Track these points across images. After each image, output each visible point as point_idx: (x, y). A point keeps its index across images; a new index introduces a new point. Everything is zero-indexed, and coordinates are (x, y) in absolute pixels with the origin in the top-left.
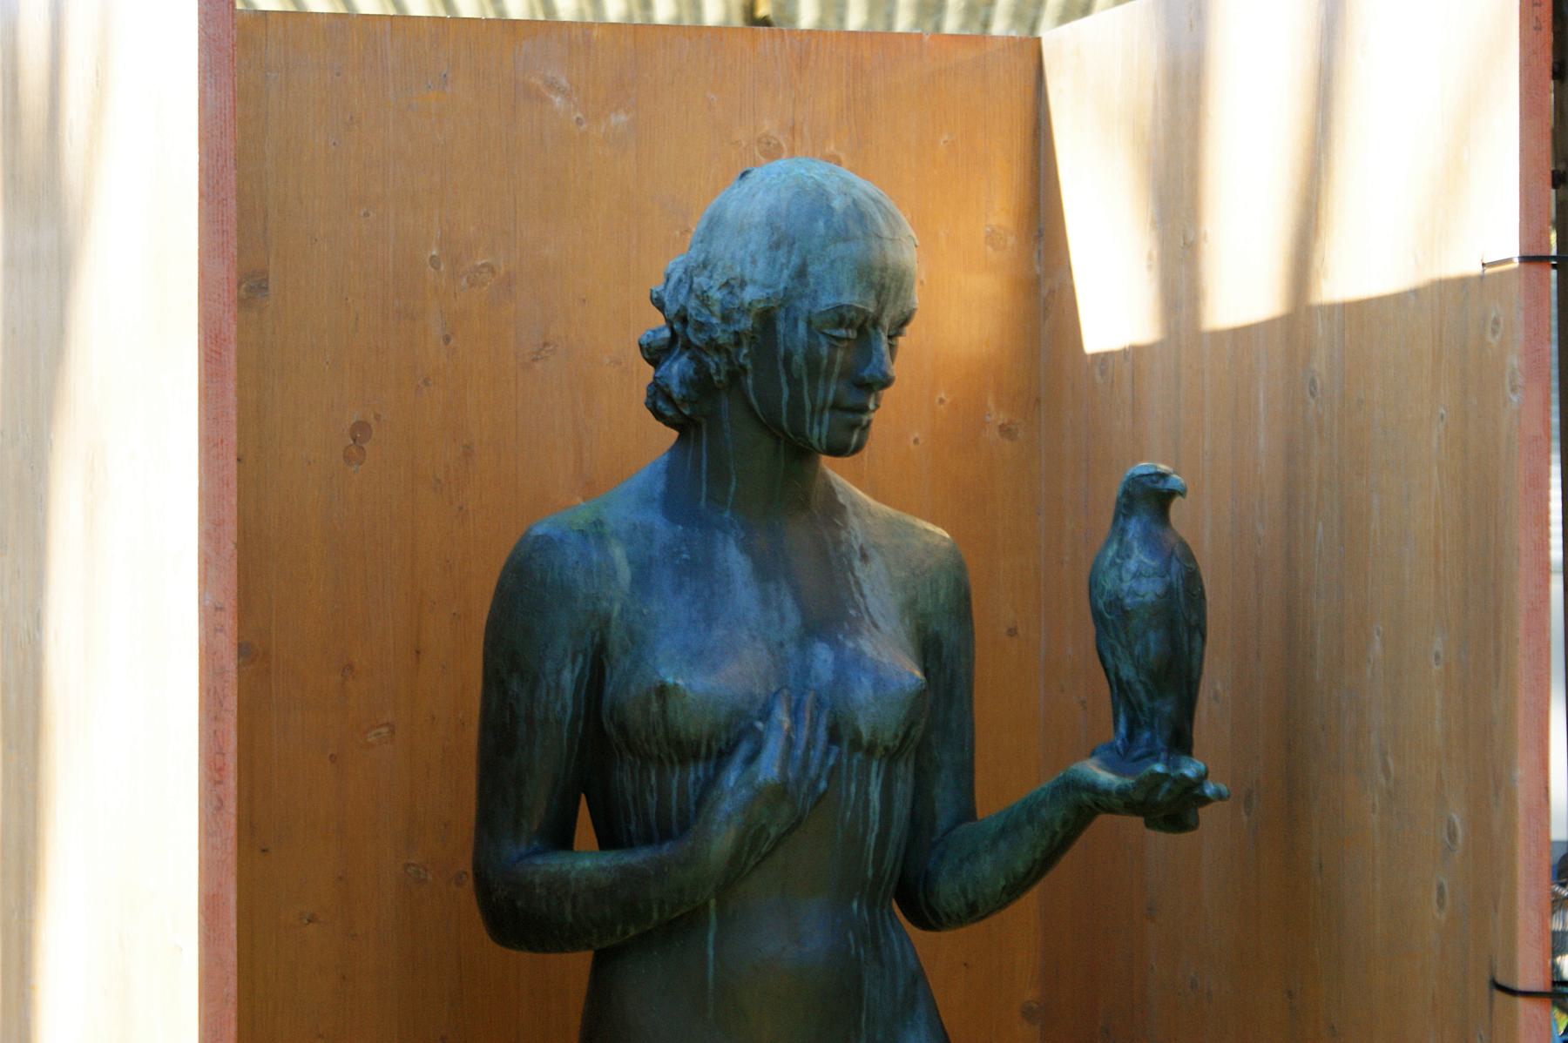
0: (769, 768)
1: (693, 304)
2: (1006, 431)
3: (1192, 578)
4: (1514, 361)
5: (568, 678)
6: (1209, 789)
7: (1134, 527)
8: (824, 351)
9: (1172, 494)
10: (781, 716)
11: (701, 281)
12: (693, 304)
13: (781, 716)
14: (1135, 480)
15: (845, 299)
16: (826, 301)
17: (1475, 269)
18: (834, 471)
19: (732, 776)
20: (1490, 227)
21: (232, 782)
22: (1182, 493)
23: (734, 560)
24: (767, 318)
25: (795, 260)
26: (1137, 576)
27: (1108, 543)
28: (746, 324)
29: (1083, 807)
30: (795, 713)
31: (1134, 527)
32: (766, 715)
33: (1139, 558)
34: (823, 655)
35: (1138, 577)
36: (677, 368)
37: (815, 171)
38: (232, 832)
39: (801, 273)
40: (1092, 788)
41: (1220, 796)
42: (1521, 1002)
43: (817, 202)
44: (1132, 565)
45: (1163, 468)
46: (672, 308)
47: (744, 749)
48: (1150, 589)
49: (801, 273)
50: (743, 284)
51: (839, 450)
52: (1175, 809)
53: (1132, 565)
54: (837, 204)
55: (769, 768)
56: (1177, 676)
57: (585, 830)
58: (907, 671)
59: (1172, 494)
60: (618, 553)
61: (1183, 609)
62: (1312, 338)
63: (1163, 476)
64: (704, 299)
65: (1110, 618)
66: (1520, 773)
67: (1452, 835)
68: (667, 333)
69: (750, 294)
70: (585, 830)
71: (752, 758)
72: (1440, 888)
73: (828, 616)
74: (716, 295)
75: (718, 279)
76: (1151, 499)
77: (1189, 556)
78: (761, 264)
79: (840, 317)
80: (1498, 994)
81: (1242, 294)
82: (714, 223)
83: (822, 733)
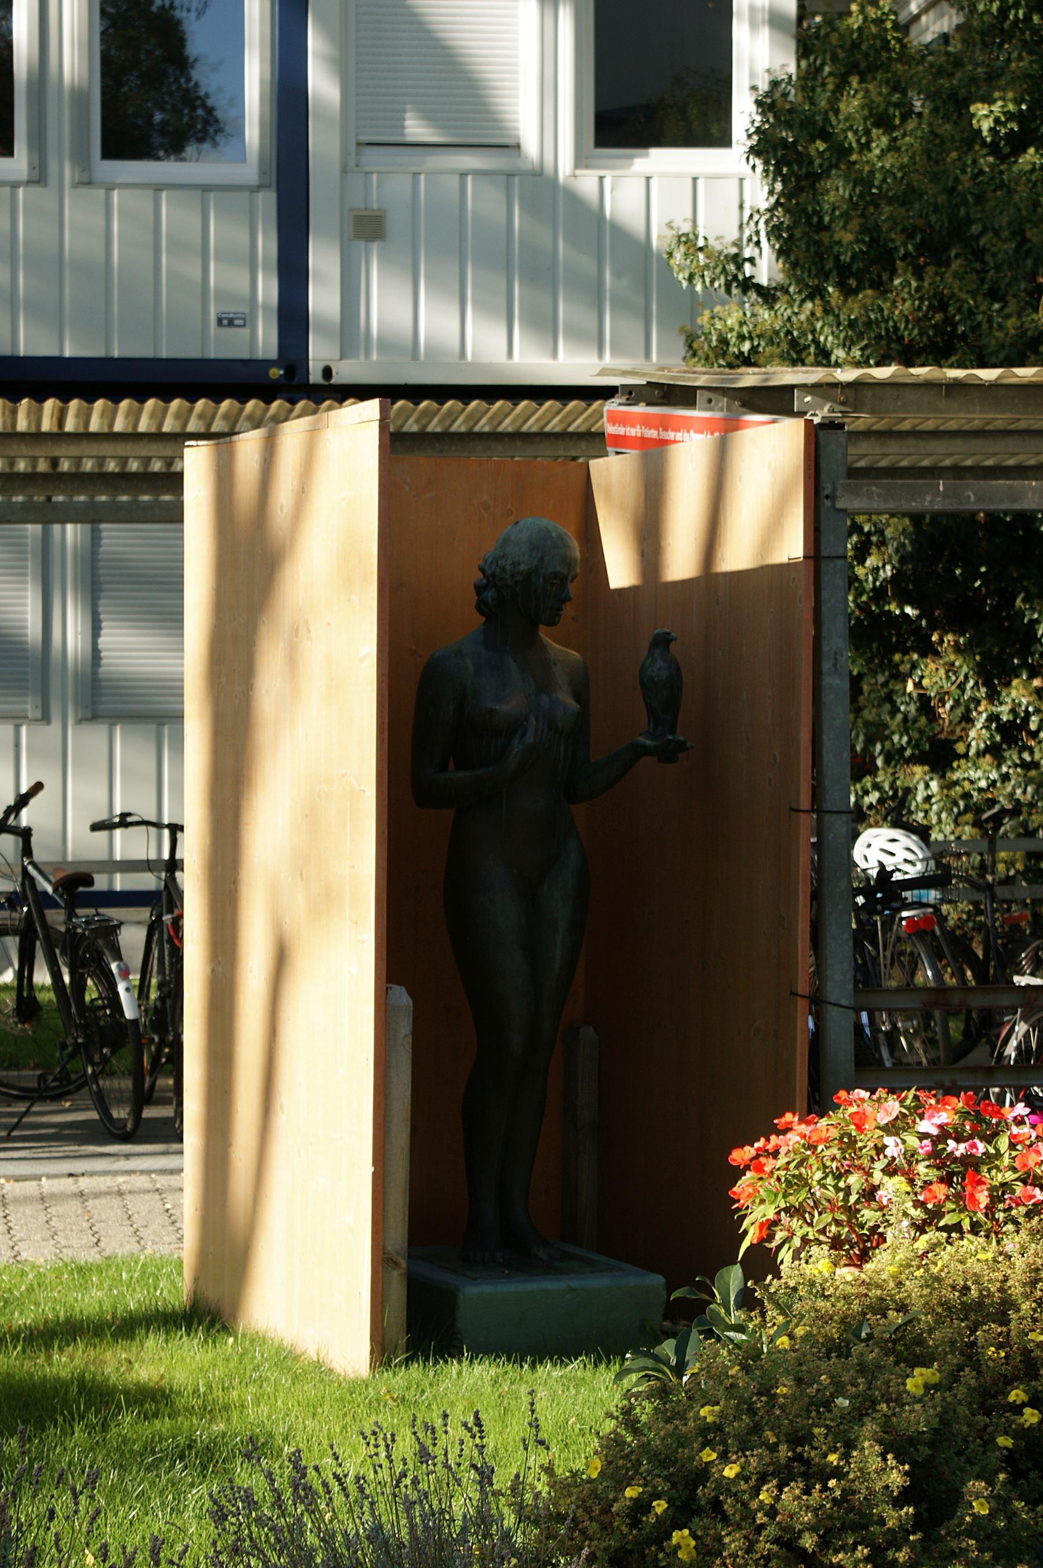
0: (530, 738)
1: (498, 570)
2: (574, 619)
3: (678, 670)
4: (801, 592)
5: (451, 707)
6: (689, 745)
7: (657, 653)
8: (549, 588)
9: (672, 640)
10: (532, 720)
11: (501, 562)
12: (498, 570)
13: (532, 720)
14: (658, 635)
15: (558, 569)
16: (551, 570)
17: (785, 560)
18: (544, 634)
19: (516, 741)
20: (792, 546)
21: (386, 733)
22: (675, 640)
23: (511, 664)
24: (528, 576)
25: (539, 555)
26: (659, 669)
27: (647, 658)
28: (520, 578)
29: (638, 752)
30: (537, 720)
31: (657, 653)
32: (527, 720)
33: (660, 663)
34: (544, 698)
35: (659, 669)
36: (490, 595)
37: (544, 522)
38: (386, 750)
39: (542, 560)
40: (644, 746)
41: (692, 748)
42: (802, 815)
43: (546, 534)
44: (657, 666)
45: (667, 630)
46: (489, 572)
47: (520, 732)
48: (664, 674)
49: (542, 560)
50: (519, 564)
51: (551, 623)
52: (668, 754)
53: (657, 666)
54: (554, 534)
55: (530, 738)
56: (672, 705)
57: (451, 766)
58: (573, 705)
59: (672, 640)
60: (469, 662)
61: (675, 682)
62: (709, 580)
63: (669, 634)
64: (503, 569)
65: (647, 685)
66: (802, 735)
67: (775, 759)
68: (485, 581)
69: (522, 567)
70: (451, 766)
71: (524, 735)
72: (770, 780)
73: (545, 685)
74: (508, 567)
75: (509, 561)
76: (662, 641)
77: (677, 663)
78: (526, 557)
79: (556, 575)
80: (793, 813)
81: (681, 563)
82: (506, 541)
83: (546, 726)
